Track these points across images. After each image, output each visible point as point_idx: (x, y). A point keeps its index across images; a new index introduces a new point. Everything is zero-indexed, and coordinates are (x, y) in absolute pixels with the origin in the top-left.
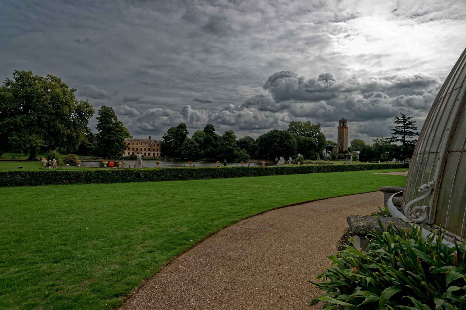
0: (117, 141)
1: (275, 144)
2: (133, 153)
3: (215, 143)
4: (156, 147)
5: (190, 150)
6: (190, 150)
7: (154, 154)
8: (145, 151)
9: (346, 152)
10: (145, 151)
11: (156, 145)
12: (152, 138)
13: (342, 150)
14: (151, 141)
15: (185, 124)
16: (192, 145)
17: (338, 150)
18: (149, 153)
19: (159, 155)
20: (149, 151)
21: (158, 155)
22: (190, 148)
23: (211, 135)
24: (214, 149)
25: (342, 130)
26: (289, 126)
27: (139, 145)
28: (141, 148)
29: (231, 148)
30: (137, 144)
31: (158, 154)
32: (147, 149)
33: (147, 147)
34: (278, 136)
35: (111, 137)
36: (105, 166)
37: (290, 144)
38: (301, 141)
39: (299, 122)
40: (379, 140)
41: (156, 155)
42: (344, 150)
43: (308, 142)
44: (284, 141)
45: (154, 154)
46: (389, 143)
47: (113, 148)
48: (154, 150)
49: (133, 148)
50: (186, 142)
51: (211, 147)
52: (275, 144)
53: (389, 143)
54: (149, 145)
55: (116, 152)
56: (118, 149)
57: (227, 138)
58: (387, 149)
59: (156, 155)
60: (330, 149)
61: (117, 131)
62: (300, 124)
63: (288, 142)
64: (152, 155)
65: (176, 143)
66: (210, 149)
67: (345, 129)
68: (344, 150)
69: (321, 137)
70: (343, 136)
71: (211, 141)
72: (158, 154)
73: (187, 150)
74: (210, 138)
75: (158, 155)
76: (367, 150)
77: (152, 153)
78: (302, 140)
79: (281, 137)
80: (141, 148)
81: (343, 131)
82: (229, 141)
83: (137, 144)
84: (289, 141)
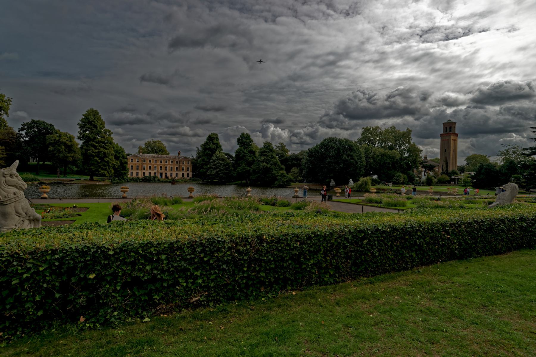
0: (98, 156)
1: (329, 159)
2: (155, 173)
3: (251, 159)
4: (186, 165)
5: (218, 170)
6: (218, 170)
7: (183, 174)
8: (171, 170)
9: (454, 173)
10: (171, 170)
11: (186, 163)
12: (181, 155)
13: (447, 170)
14: (179, 158)
15: (216, 135)
16: (221, 162)
17: (441, 171)
18: (177, 174)
19: (190, 176)
20: (177, 170)
21: (188, 176)
22: (218, 167)
23: (245, 148)
24: (247, 168)
25: (447, 138)
26: (363, 134)
27: (164, 163)
28: (166, 167)
29: (268, 166)
30: (161, 162)
31: (188, 174)
32: (174, 168)
33: (175, 165)
34: (333, 147)
35: (89, 150)
36: (338, 195)
37: (353, 158)
38: (378, 156)
39: (377, 128)
40: (511, 153)
41: (185, 176)
42: (450, 169)
43: (389, 157)
44: (342, 155)
45: (183, 174)
46: (529, 155)
47: (93, 165)
48: (183, 170)
49: (155, 167)
50: (214, 158)
51: (243, 165)
52: (329, 159)
53: (529, 155)
54: (177, 163)
55: (97, 170)
56: (100, 167)
57: (265, 152)
58: (525, 167)
59: (185, 176)
60: (431, 168)
61: (98, 142)
62: (379, 131)
63: (348, 156)
64: (181, 176)
65: (203, 160)
66: (243, 167)
67: (452, 137)
68: (450, 169)
69: (414, 151)
70: (449, 147)
71: (244, 156)
72: (188, 174)
73: (215, 169)
74: (244, 152)
75: (188, 176)
76: (486, 169)
77: (181, 173)
78: (378, 153)
79: (339, 149)
80: (166, 167)
81: (448, 141)
82: (267, 156)
83: (161, 162)
84: (351, 156)
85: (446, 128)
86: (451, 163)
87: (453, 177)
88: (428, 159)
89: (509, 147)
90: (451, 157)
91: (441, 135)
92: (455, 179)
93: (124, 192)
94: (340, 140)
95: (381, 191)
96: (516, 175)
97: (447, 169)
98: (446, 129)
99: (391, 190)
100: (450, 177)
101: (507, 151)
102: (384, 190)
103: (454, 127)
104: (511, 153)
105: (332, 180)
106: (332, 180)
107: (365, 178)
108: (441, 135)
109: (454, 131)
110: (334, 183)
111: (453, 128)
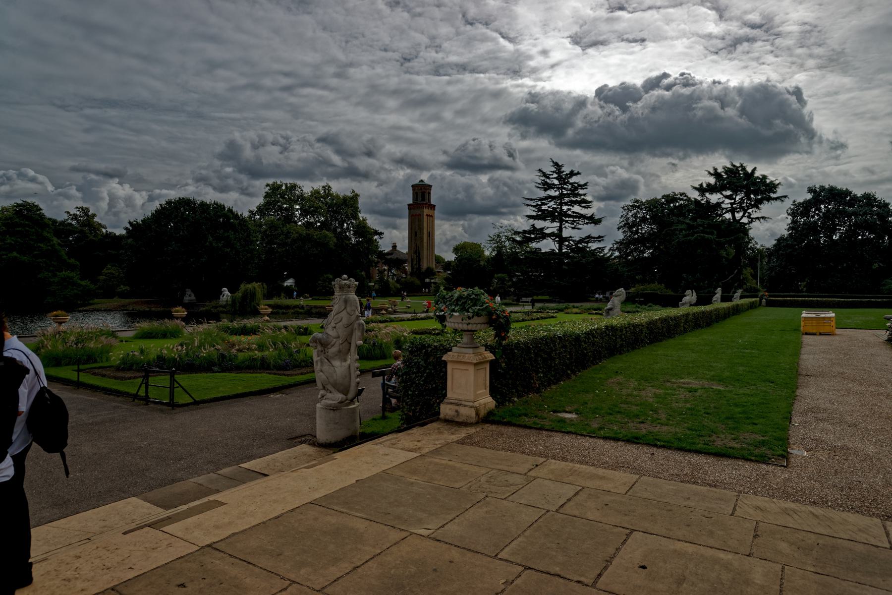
13: (419, 268)
40: (503, 239)
67: (426, 211)
68: (425, 266)
81: (420, 216)
85: (417, 193)
86: (425, 256)
87: (427, 280)
88: (96, 219)
89: (501, 230)
90: (425, 245)
91: (409, 205)
92: (431, 283)
93: (61, 323)
94: (203, 204)
95: (281, 311)
96: (499, 275)
97: (419, 265)
98: (415, 195)
99: (303, 307)
100: (422, 280)
101: (499, 236)
102: (288, 307)
103: (429, 193)
104: (503, 239)
105: (189, 292)
106: (189, 292)
107: (250, 286)
108: (409, 205)
109: (429, 200)
110: (193, 297)
111: (426, 195)
